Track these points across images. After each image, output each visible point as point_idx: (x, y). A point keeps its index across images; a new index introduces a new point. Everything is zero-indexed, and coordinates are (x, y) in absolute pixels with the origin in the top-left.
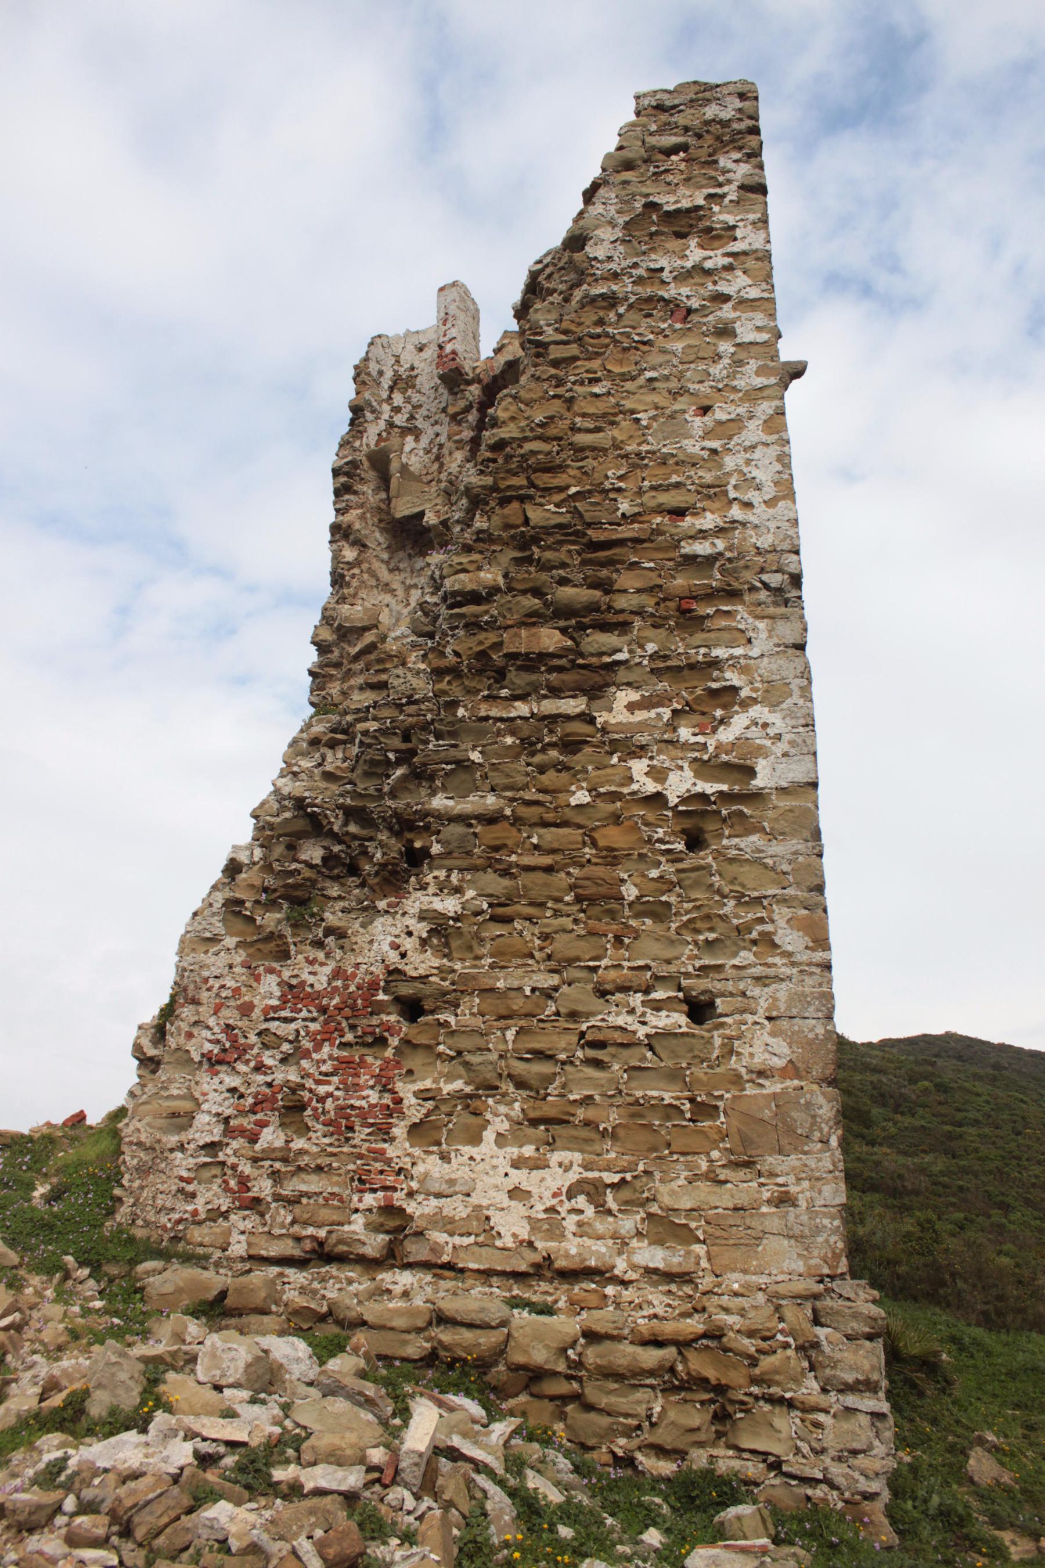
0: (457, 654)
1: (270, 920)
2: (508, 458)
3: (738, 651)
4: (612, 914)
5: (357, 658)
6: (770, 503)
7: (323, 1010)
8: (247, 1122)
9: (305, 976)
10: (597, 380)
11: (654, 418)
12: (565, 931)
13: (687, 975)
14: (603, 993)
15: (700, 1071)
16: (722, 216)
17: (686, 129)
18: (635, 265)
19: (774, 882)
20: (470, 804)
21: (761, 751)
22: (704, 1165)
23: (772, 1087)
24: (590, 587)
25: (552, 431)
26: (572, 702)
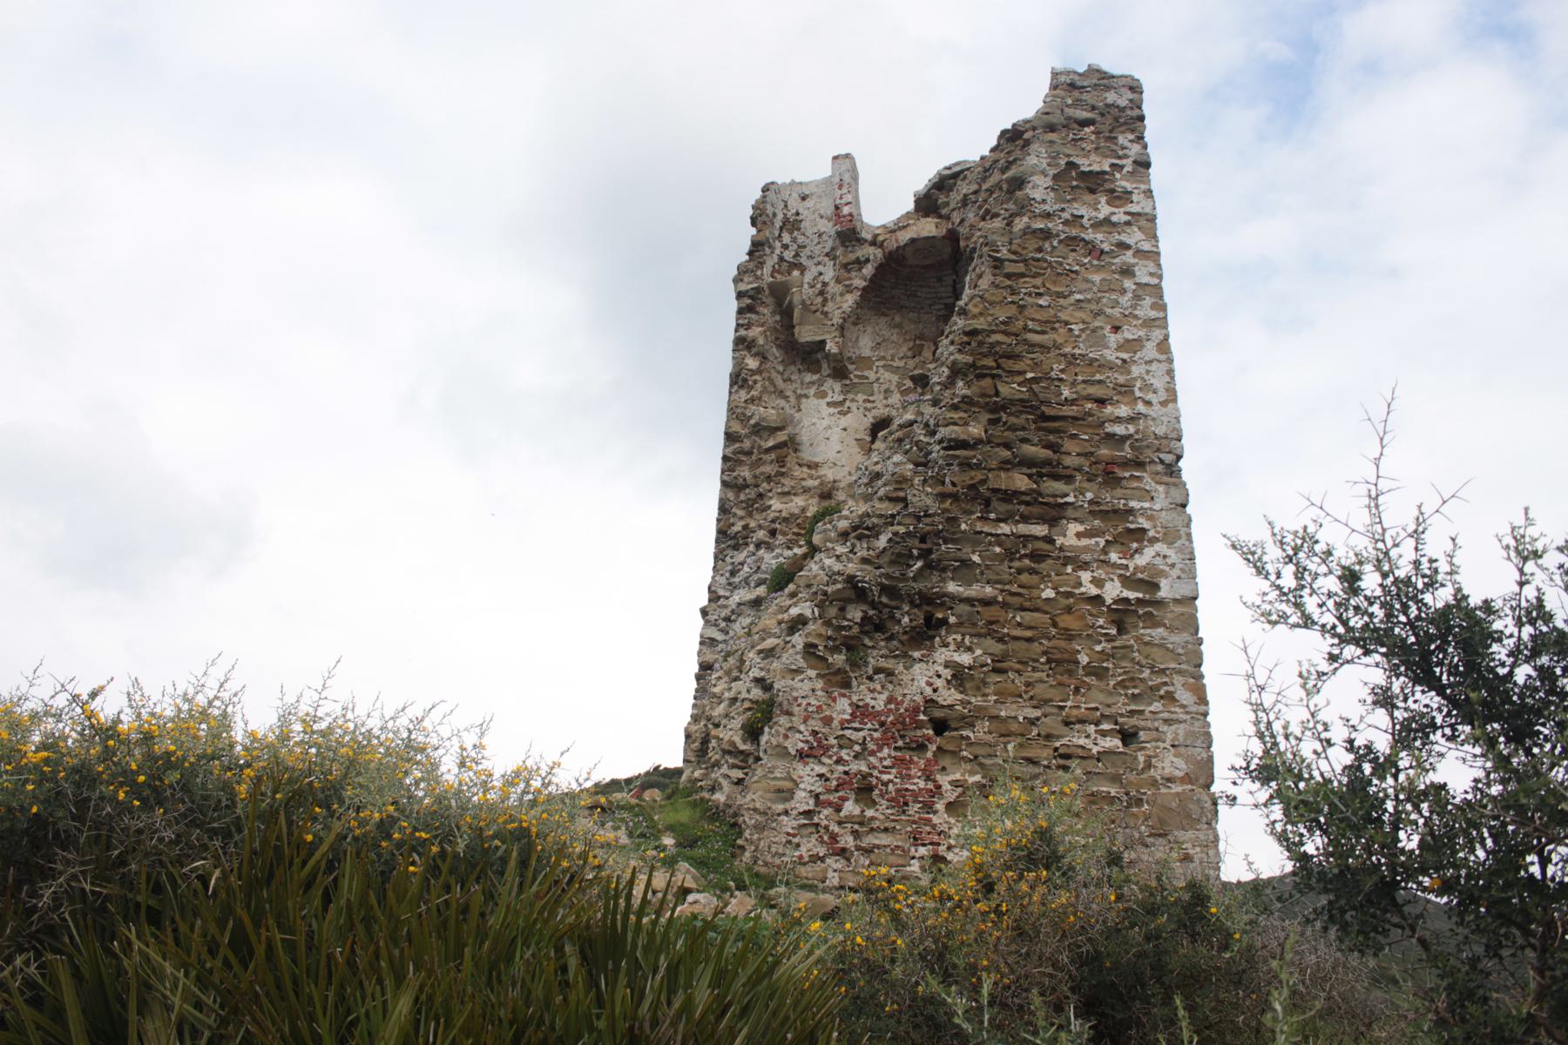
0: (954, 484)
1: (839, 659)
2: (981, 344)
3: (1146, 505)
4: (1070, 673)
5: (768, 451)
6: (1164, 404)
7: (882, 724)
8: (833, 797)
9: (868, 700)
10: (1039, 295)
11: (1082, 330)
12: (1042, 681)
13: (1122, 715)
14: (1067, 723)
15: (1132, 777)
16: (1123, 184)
17: (1093, 108)
18: (1063, 210)
19: (1175, 660)
20: (974, 591)
21: (1162, 574)
22: (1137, 835)
23: (1176, 788)
24: (1044, 447)
25: (1012, 329)
26: (1039, 528)
